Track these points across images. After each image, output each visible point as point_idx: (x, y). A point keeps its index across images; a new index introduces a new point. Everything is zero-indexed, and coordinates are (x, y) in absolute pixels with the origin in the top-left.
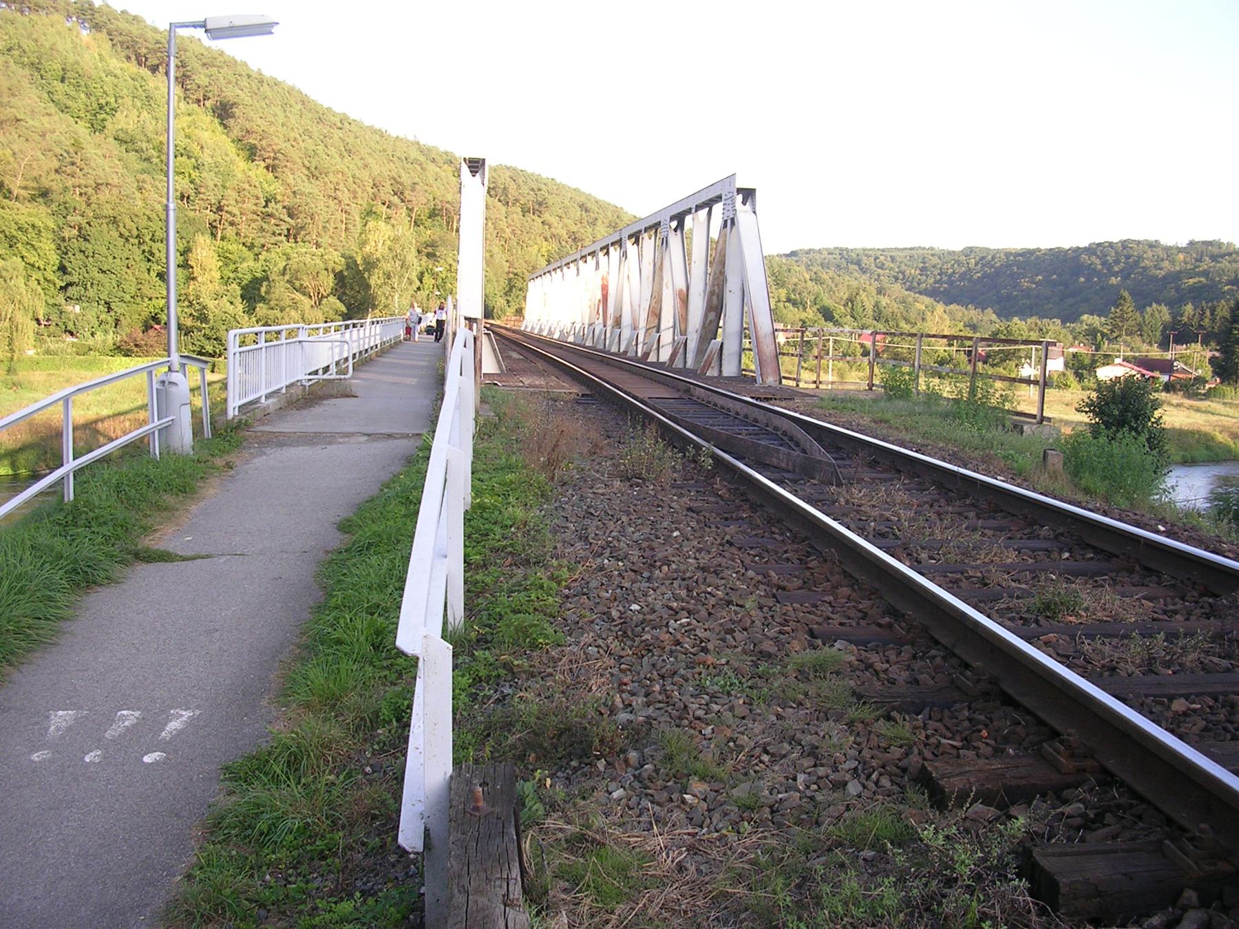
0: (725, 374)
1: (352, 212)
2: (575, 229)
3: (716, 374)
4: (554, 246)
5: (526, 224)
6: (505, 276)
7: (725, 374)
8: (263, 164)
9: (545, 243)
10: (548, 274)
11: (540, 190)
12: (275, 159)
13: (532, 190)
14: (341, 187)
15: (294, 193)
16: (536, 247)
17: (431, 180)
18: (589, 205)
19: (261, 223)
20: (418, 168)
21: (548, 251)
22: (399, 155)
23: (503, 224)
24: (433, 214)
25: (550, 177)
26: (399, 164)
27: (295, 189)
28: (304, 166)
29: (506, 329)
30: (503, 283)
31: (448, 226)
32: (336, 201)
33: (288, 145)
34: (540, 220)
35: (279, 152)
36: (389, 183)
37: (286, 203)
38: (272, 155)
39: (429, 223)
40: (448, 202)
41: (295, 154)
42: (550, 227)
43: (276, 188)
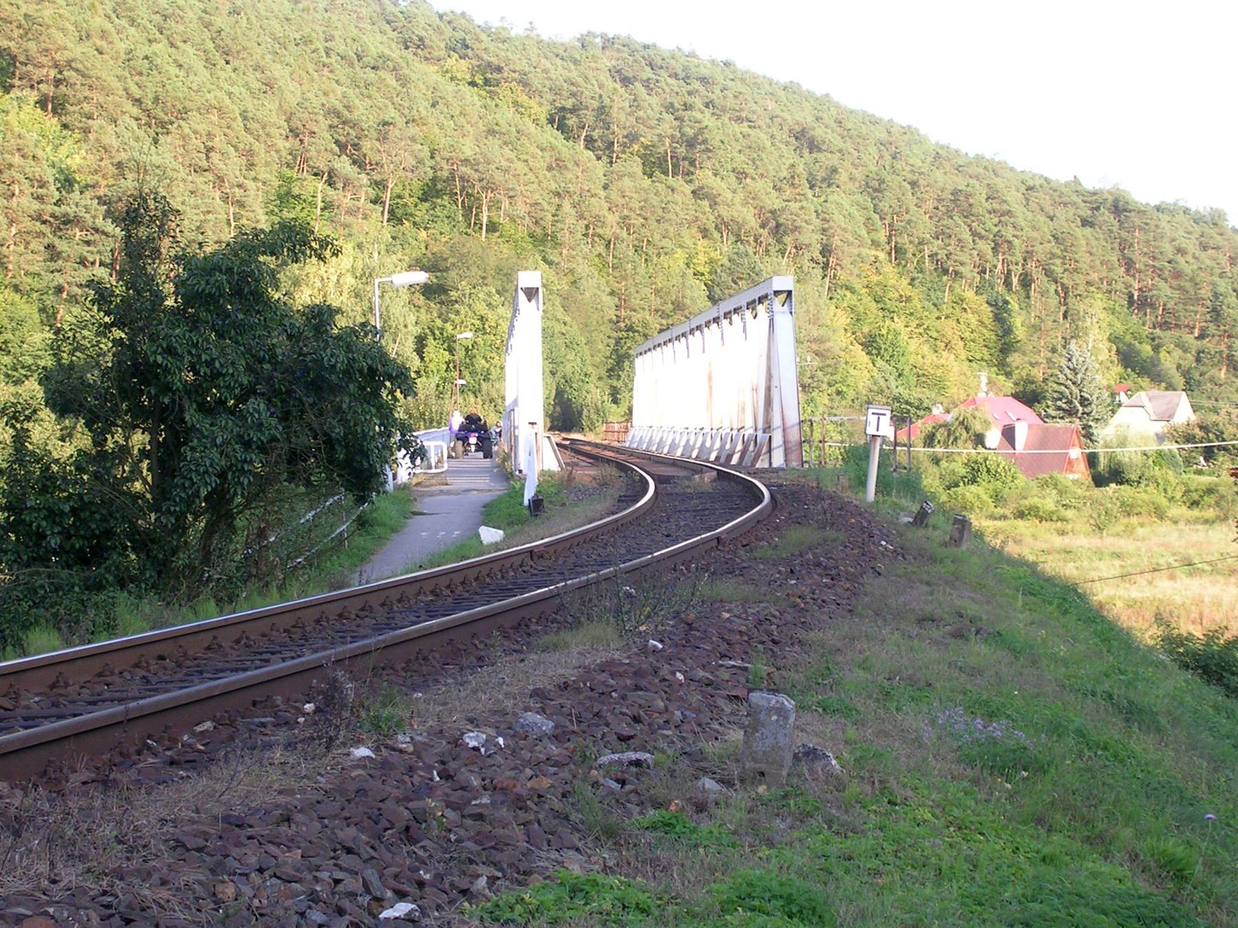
0: (775, 465)
1: (249, 201)
2: (773, 201)
3: (766, 466)
4: (724, 249)
5: (655, 201)
6: (607, 329)
7: (775, 465)
8: (33, 96)
9: (702, 244)
10: (698, 333)
11: (687, 107)
12: (58, 82)
13: (670, 108)
14: (219, 142)
15: (119, 165)
16: (680, 255)
17: (423, 107)
18: (819, 132)
19: (50, 238)
20: (391, 80)
21: (711, 262)
22: (341, 48)
23: (598, 206)
24: (430, 193)
25: (720, 57)
26: (342, 72)
27: (123, 156)
28: (129, 96)
29: (606, 447)
30: (603, 347)
31: (467, 217)
32: (210, 176)
33: (86, 49)
34: (688, 189)
35: (69, 63)
36: (324, 123)
37: (102, 191)
38: (53, 73)
39: (422, 211)
40: (466, 161)
41: (107, 71)
42: (714, 204)
43: (76, 158)
